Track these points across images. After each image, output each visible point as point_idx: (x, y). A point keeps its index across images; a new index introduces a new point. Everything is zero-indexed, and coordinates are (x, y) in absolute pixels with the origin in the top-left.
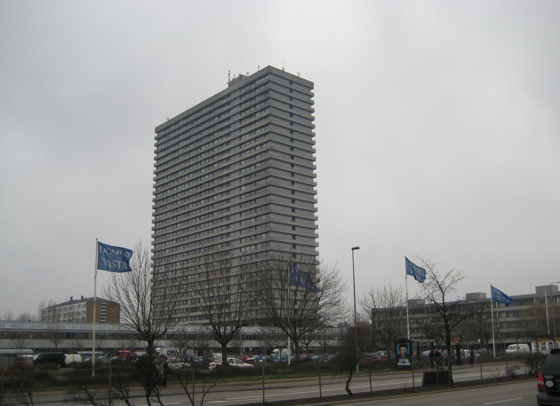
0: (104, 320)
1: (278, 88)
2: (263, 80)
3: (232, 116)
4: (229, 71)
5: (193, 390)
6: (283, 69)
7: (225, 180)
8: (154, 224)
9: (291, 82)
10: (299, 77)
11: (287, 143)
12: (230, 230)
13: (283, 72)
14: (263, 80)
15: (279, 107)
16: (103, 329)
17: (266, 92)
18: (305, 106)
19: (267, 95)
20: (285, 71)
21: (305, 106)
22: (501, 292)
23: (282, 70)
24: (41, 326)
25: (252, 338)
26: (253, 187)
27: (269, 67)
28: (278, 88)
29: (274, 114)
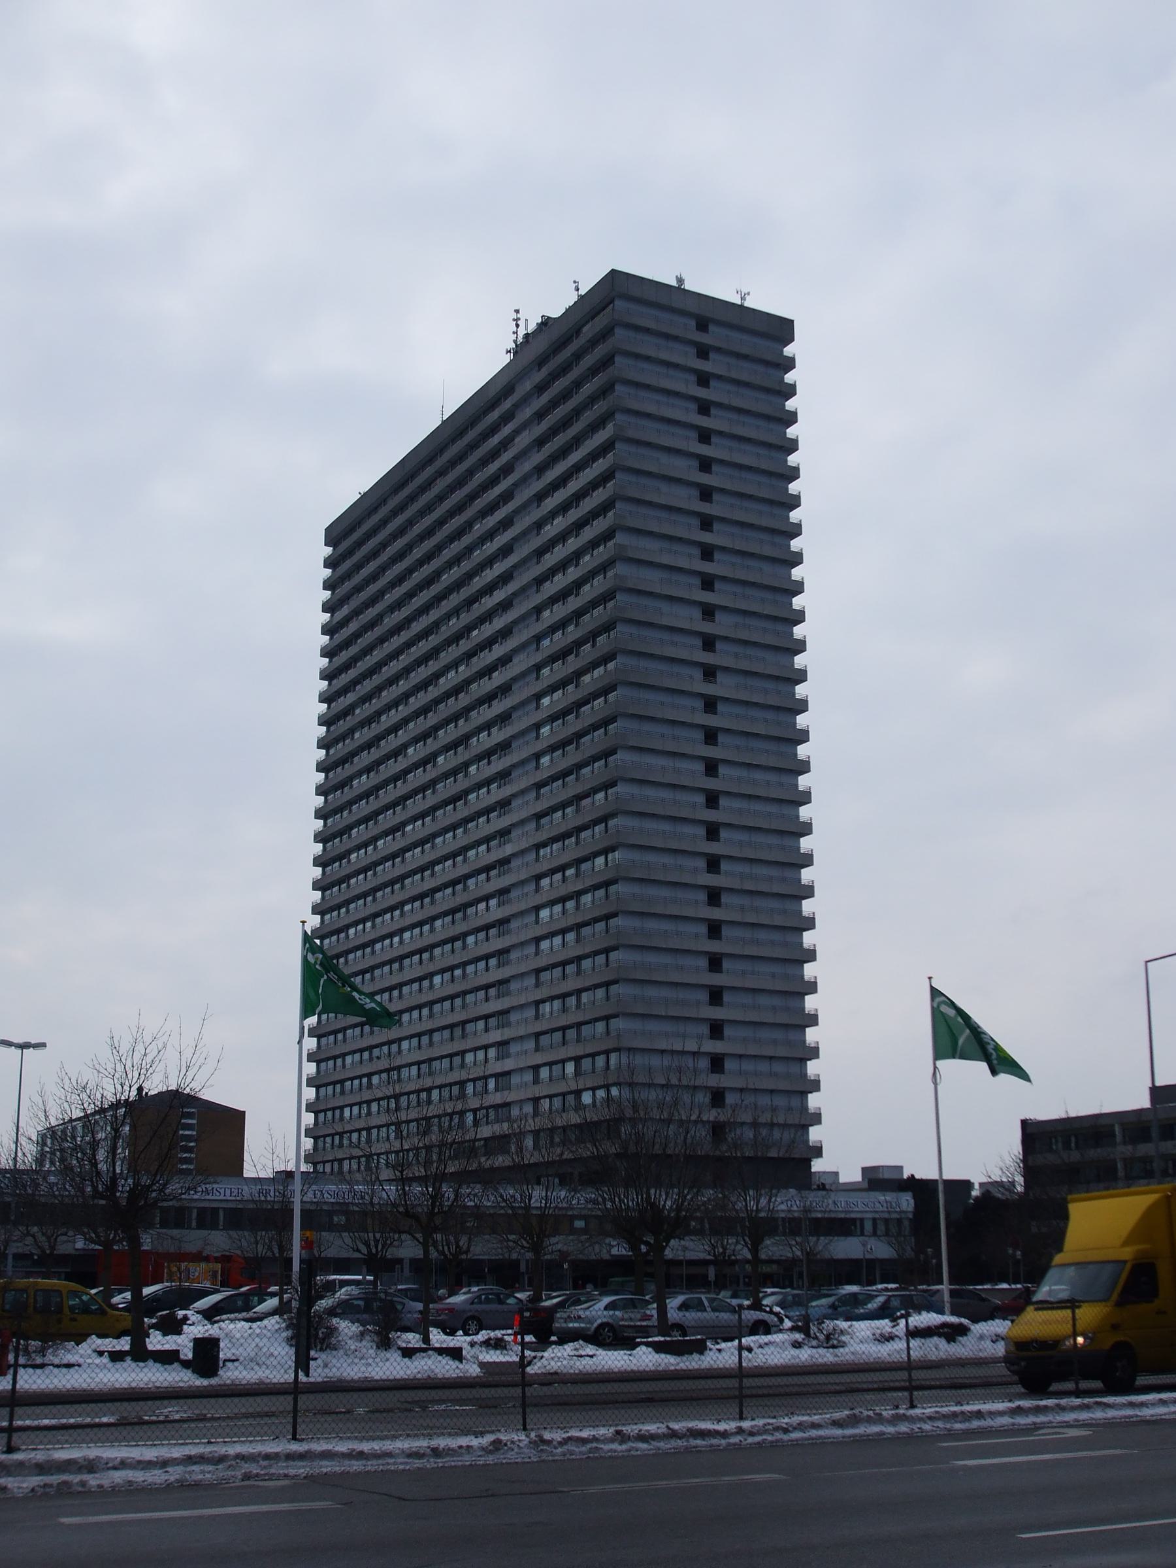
0: (191, 1163)
1: (648, 345)
2: (600, 323)
3: (516, 458)
4: (517, 311)
5: (910, 1375)
6: (680, 280)
7: (498, 678)
8: (321, 845)
9: (703, 325)
10: (742, 306)
11: (684, 534)
12: (509, 849)
13: (679, 290)
14: (600, 323)
15: (651, 408)
16: (222, 1197)
17: (606, 362)
18: (760, 404)
19: (611, 372)
20: (688, 286)
21: (760, 404)
22: (960, 1012)
23: (674, 283)
24: (222, 1191)
25: (194, 1224)
26: (572, 694)
27: (614, 277)
28: (648, 345)
29: (631, 434)
